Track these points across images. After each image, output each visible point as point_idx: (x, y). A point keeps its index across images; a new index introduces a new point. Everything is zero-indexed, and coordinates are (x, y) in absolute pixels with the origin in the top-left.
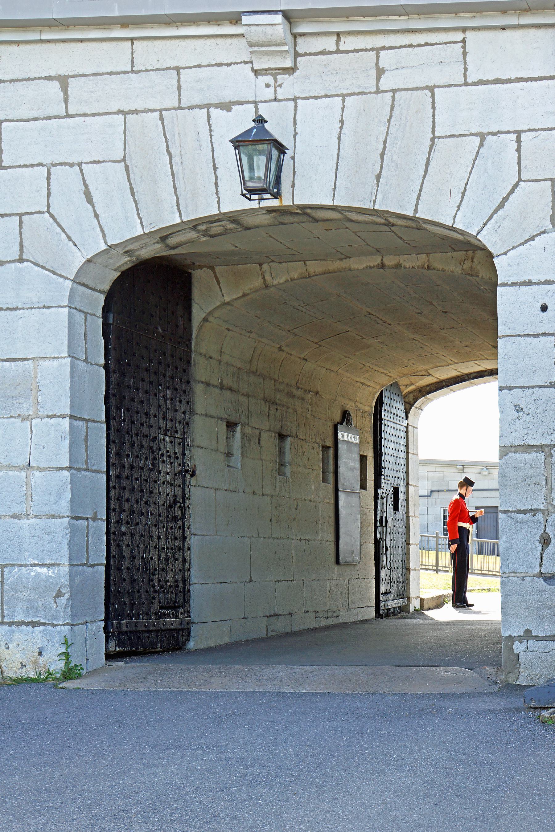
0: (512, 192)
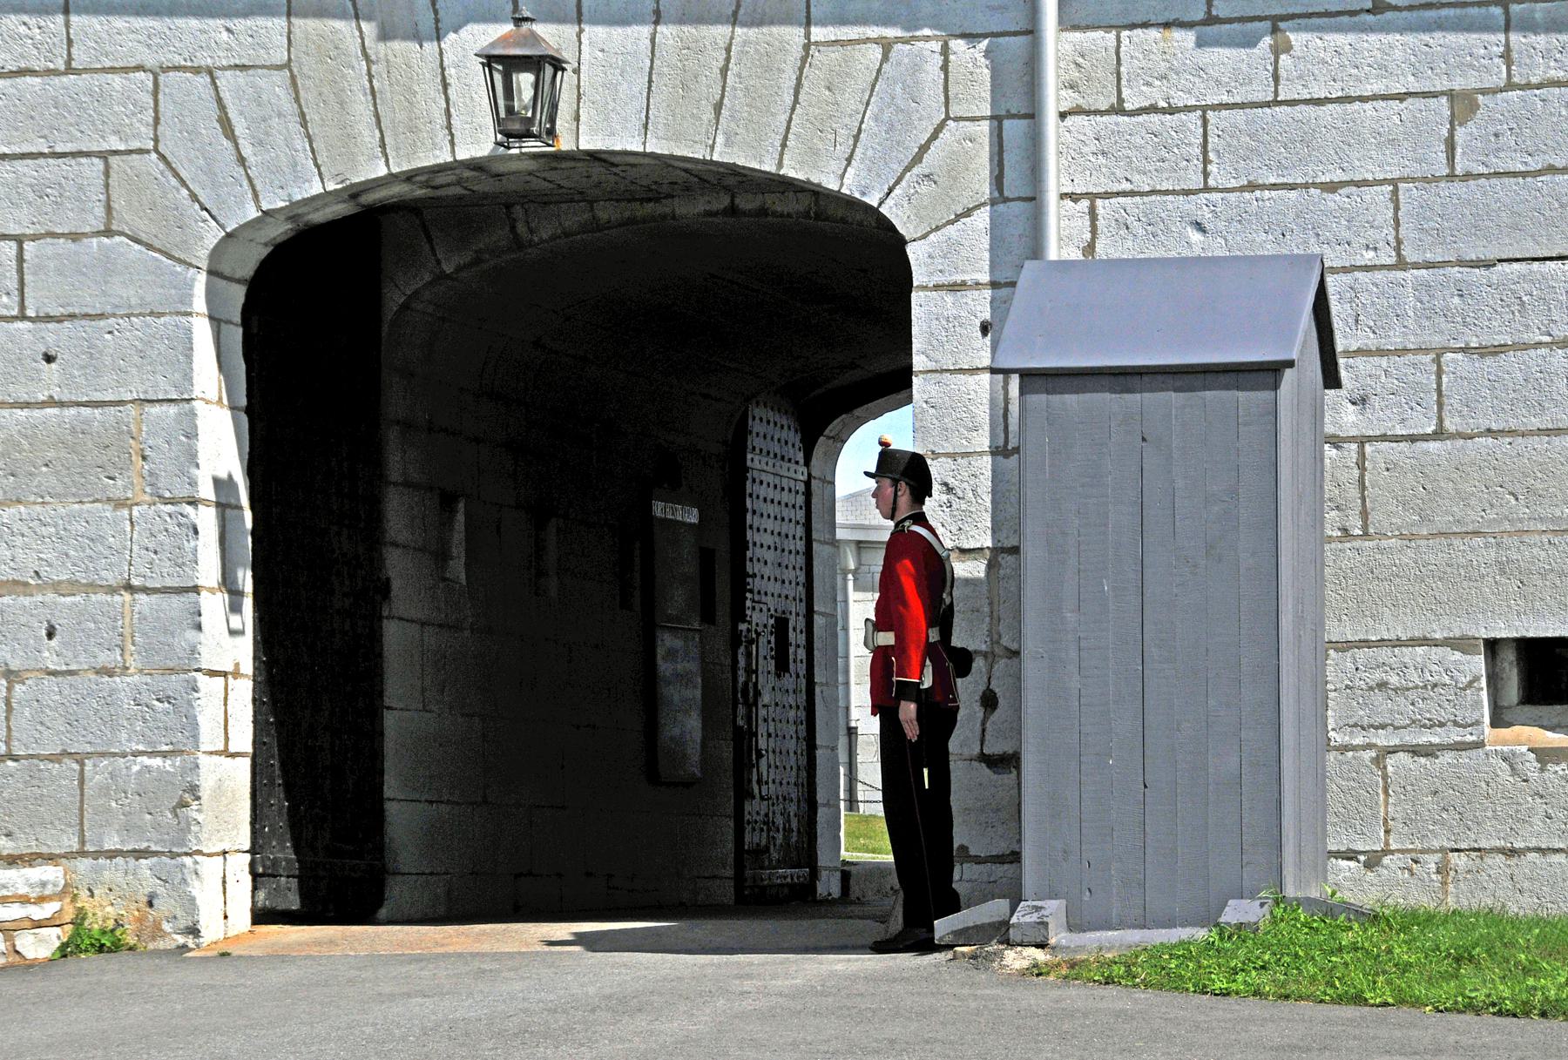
0: (935, 136)
